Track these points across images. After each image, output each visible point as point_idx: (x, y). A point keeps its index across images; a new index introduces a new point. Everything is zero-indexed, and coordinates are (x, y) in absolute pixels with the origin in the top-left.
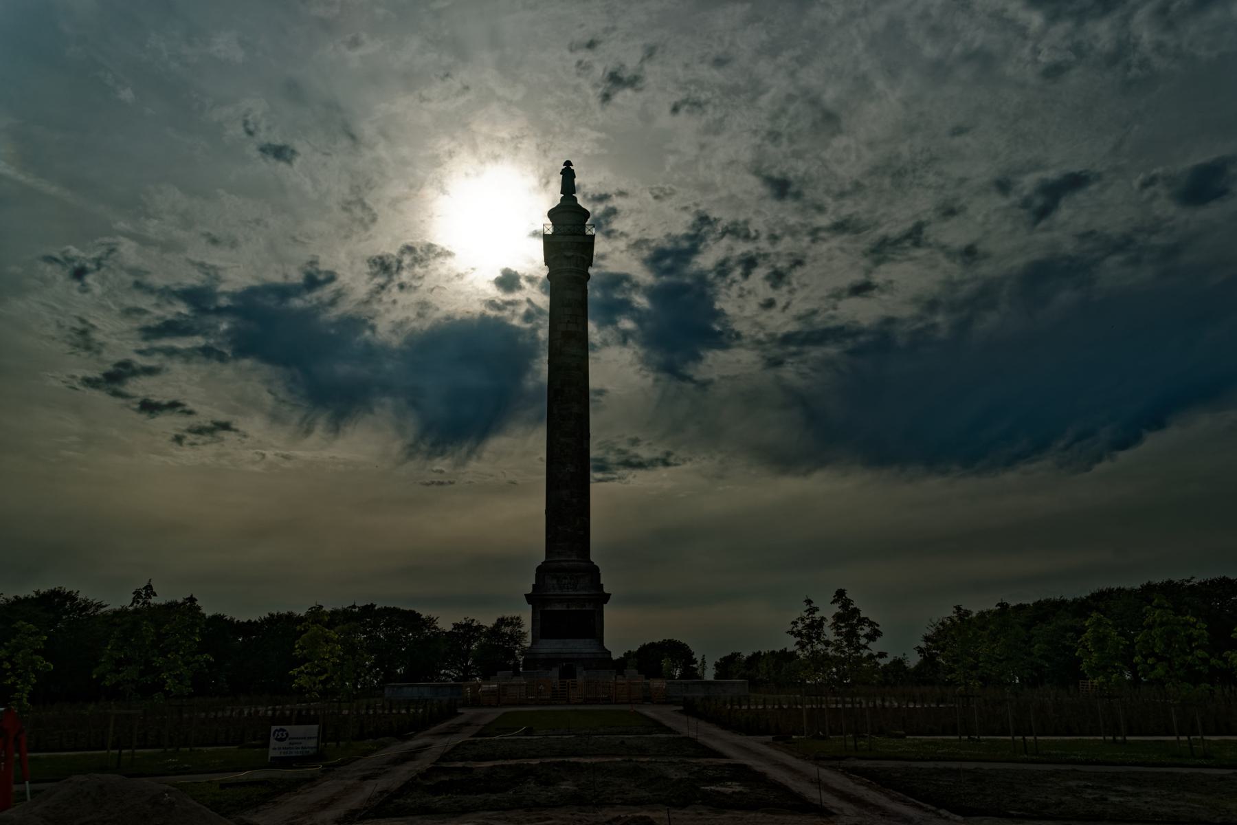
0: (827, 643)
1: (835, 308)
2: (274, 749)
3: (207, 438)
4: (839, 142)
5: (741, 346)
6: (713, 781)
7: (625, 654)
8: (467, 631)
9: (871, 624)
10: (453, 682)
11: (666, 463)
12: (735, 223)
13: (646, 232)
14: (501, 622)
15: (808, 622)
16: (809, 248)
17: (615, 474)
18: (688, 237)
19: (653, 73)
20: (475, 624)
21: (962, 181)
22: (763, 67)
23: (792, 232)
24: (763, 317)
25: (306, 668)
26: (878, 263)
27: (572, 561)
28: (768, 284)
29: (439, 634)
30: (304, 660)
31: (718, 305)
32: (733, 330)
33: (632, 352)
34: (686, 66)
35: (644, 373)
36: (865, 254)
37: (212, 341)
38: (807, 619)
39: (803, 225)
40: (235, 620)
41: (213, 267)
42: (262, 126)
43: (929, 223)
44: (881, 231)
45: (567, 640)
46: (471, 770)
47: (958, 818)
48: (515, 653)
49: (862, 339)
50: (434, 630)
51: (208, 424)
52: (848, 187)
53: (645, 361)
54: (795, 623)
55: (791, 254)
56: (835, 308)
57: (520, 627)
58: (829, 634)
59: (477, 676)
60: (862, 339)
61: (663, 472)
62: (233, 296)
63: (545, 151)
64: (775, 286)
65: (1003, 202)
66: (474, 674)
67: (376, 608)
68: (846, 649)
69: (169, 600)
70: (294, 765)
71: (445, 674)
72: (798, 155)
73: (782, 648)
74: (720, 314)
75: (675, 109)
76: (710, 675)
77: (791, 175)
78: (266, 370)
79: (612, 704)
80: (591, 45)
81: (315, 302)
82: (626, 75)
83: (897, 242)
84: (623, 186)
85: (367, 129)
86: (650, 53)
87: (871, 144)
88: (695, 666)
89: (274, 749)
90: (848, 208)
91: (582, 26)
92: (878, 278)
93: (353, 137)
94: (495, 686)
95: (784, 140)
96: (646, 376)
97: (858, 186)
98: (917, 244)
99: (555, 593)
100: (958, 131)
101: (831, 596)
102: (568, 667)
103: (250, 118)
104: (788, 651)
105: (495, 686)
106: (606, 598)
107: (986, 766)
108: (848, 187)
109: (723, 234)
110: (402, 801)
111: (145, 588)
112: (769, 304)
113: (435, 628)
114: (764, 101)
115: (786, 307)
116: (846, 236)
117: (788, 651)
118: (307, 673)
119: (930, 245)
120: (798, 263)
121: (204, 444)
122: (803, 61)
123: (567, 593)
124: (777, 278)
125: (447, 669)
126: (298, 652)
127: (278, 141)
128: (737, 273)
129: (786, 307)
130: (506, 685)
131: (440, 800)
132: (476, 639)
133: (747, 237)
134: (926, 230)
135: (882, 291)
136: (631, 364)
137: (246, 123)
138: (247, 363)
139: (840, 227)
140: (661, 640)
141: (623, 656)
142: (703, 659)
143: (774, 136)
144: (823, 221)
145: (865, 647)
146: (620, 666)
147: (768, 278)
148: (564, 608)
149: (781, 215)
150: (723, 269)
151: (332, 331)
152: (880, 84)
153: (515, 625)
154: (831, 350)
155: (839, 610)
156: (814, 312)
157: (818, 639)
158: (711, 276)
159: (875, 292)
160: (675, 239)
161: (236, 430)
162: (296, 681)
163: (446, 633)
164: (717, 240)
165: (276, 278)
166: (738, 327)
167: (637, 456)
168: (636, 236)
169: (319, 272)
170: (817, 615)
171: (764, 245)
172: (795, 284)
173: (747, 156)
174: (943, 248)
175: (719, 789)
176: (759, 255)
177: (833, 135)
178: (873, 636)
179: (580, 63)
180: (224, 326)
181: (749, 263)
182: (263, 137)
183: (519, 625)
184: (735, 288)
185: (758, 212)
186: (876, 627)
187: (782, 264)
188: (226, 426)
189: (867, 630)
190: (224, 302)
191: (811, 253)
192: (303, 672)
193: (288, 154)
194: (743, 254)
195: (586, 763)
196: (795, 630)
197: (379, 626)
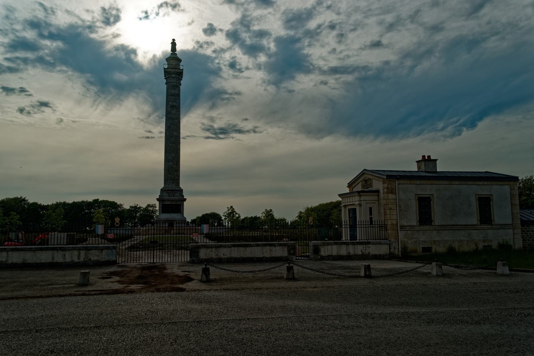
7: (197, 217)
8: (135, 209)
9: (238, 214)
11: (255, 132)
15: (227, 213)
20: (138, 206)
27: (173, 187)
29: (124, 210)
40: (42, 205)
45: (171, 214)
48: (154, 217)
50: (122, 209)
54: (224, 213)
60: (370, 73)
64: (340, 42)
67: (99, 200)
69: (15, 197)
73: (255, 215)
92: (385, 41)
102: (171, 223)
104: (257, 217)
113: (123, 208)
117: (257, 217)
140: (210, 213)
141: (196, 218)
148: (170, 203)
154: (349, 78)
163: (127, 210)
183: (155, 207)
197: (101, 207)
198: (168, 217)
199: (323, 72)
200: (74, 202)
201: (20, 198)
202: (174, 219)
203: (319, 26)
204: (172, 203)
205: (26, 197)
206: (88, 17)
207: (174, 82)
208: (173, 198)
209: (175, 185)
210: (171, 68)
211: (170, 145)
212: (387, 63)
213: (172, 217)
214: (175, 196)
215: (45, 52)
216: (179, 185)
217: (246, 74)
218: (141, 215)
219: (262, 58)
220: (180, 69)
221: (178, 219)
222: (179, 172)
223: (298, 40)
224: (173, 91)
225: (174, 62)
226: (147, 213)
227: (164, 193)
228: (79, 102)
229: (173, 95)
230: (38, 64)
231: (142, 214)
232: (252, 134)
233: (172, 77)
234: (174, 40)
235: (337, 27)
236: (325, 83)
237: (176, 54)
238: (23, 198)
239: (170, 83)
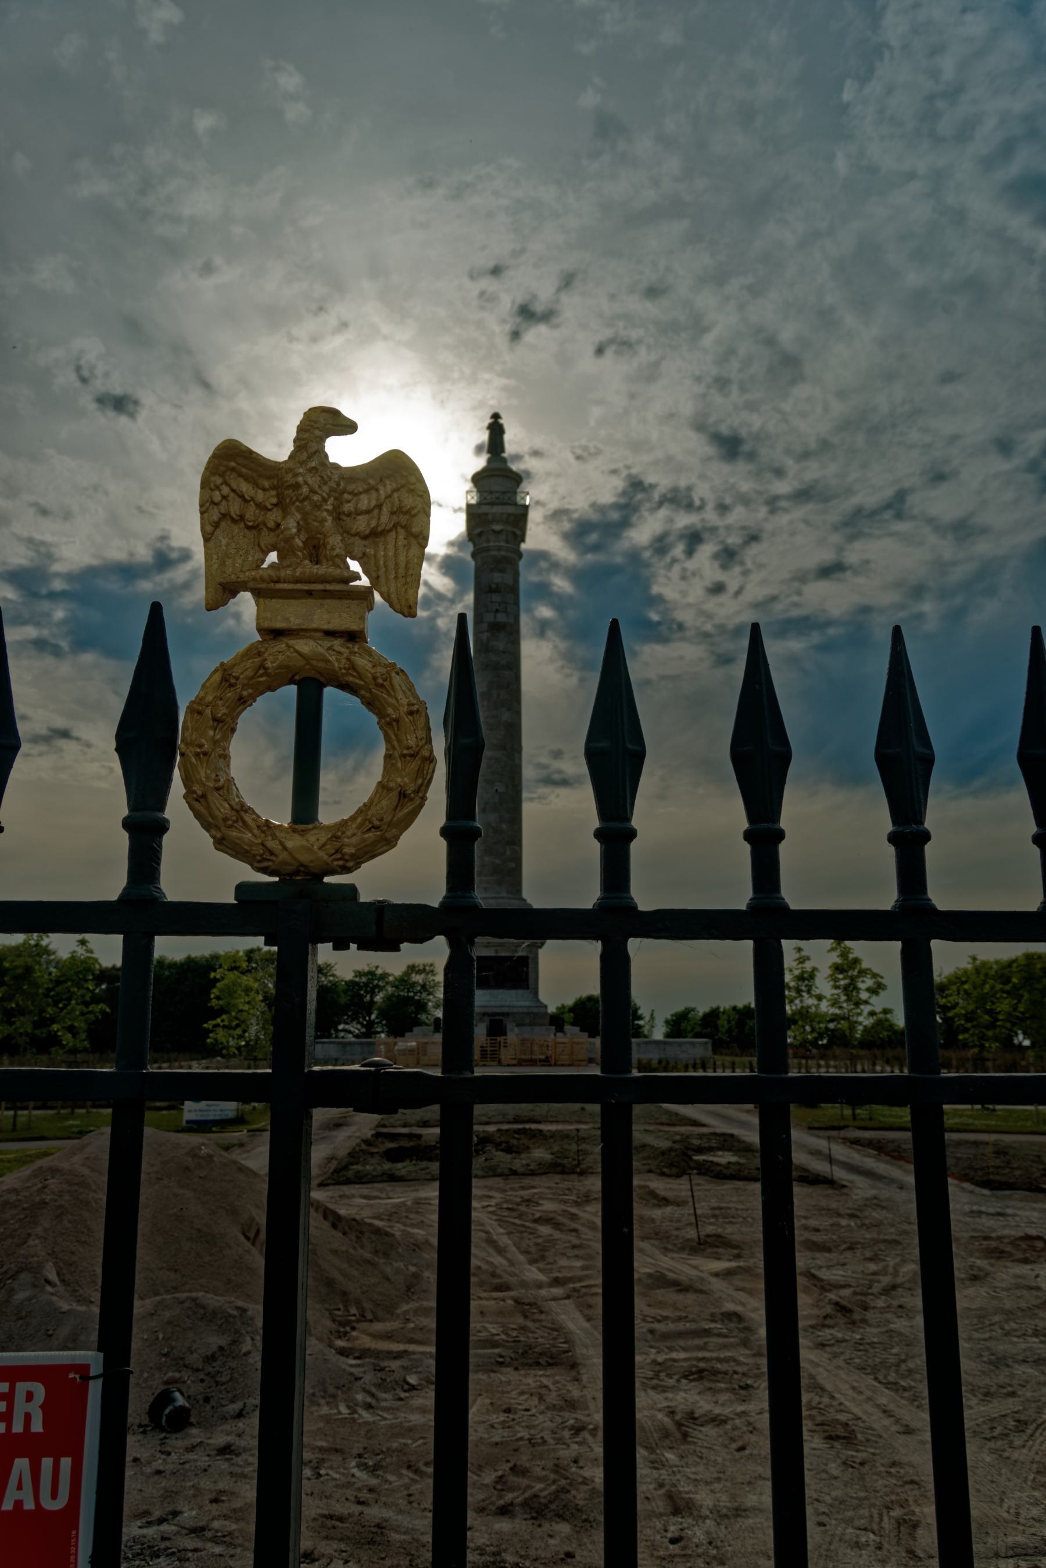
0: (820, 998)
1: (799, 593)
2: (190, 1111)
3: (43, 747)
4: (801, 391)
5: (684, 639)
6: (700, 1150)
9: (875, 975)
10: (353, 1039)
12: (675, 490)
13: (566, 500)
14: (412, 969)
15: (797, 972)
16: (766, 520)
17: (534, 792)
18: (616, 506)
19: (571, 305)
20: (379, 971)
21: (954, 439)
22: (707, 300)
23: (745, 500)
24: (711, 604)
25: (223, 1021)
26: (852, 538)
27: (503, 898)
28: (716, 564)
30: (222, 1011)
31: (655, 590)
32: (673, 621)
33: (551, 645)
34: (612, 297)
35: (567, 671)
36: (836, 528)
37: (45, 632)
39: (759, 493)
41: (43, 543)
42: (100, 369)
43: (912, 490)
44: (854, 501)
46: (419, 1136)
47: (986, 1192)
49: (832, 631)
50: (331, 978)
51: (44, 732)
52: (813, 445)
53: (568, 657)
55: (744, 528)
56: (799, 593)
57: (434, 975)
58: (823, 985)
59: (382, 1032)
62: (69, 577)
63: (442, 402)
64: (724, 567)
65: (1000, 465)
66: (379, 1029)
68: (845, 1005)
70: (214, 1129)
71: (344, 1030)
72: (752, 407)
74: (659, 599)
75: (600, 351)
76: (659, 1033)
77: (743, 432)
79: (550, 1065)
80: (496, 271)
81: (166, 585)
82: (539, 308)
83: (873, 513)
84: (538, 443)
85: (222, 376)
86: (567, 281)
87: (842, 394)
88: (641, 1023)
89: (190, 1111)
90: (813, 472)
91: (484, 248)
92: (852, 557)
93: (206, 385)
94: (414, 1044)
95: (735, 390)
96: (568, 676)
97: (825, 446)
98: (899, 516)
100: (949, 378)
103: (83, 362)
105: (414, 1044)
107: (1008, 1138)
108: (813, 445)
109: (660, 504)
110: (359, 1167)
112: (718, 589)
113: (333, 975)
114: (708, 340)
115: (738, 593)
116: (810, 506)
118: (224, 1027)
119: (914, 518)
120: (754, 538)
121: (41, 755)
122: (755, 291)
124: (728, 556)
125: (347, 1023)
126: (214, 1003)
127: (118, 391)
128: (678, 550)
129: (738, 593)
130: (427, 1043)
131: (404, 1167)
132: (381, 989)
133: (690, 507)
134: (912, 500)
135: (856, 572)
136: (551, 660)
137: (78, 369)
138: (88, 658)
139: (803, 495)
142: (652, 1015)
143: (722, 383)
144: (782, 487)
145: (866, 1002)
146: (557, 1021)
147: (716, 556)
149: (732, 480)
150: (661, 545)
151: (190, 620)
152: (850, 320)
153: (428, 973)
155: (839, 961)
156: (774, 599)
157: (809, 992)
158: (647, 554)
159: (848, 574)
160: (600, 509)
161: (78, 739)
162: (211, 1035)
164: (653, 510)
165: (117, 553)
166: (680, 616)
167: (560, 772)
168: (554, 505)
169: (171, 549)
170: (808, 966)
171: (711, 516)
172: (749, 564)
173: (688, 408)
174: (930, 521)
175: (711, 1159)
176: (705, 529)
177: (793, 382)
178: (874, 991)
179: (482, 294)
180: (59, 614)
181: (694, 539)
182: (99, 385)
183: (432, 972)
184: (677, 569)
185: (702, 477)
186: (880, 980)
187: (734, 540)
188: (65, 734)
189: (869, 982)
190: (58, 585)
191: (768, 527)
193: (130, 407)
194: (686, 527)
195: (549, 1131)
200: (189, 958)
202: (505, 1010)
207: (499, 549)
210: (492, 504)
218: (389, 998)
220: (515, 504)
221: (520, 1010)
222: (520, 846)
226: (409, 991)
229: (496, 590)
231: (393, 995)
234: (496, 416)
237: (504, 460)
239: (487, 549)
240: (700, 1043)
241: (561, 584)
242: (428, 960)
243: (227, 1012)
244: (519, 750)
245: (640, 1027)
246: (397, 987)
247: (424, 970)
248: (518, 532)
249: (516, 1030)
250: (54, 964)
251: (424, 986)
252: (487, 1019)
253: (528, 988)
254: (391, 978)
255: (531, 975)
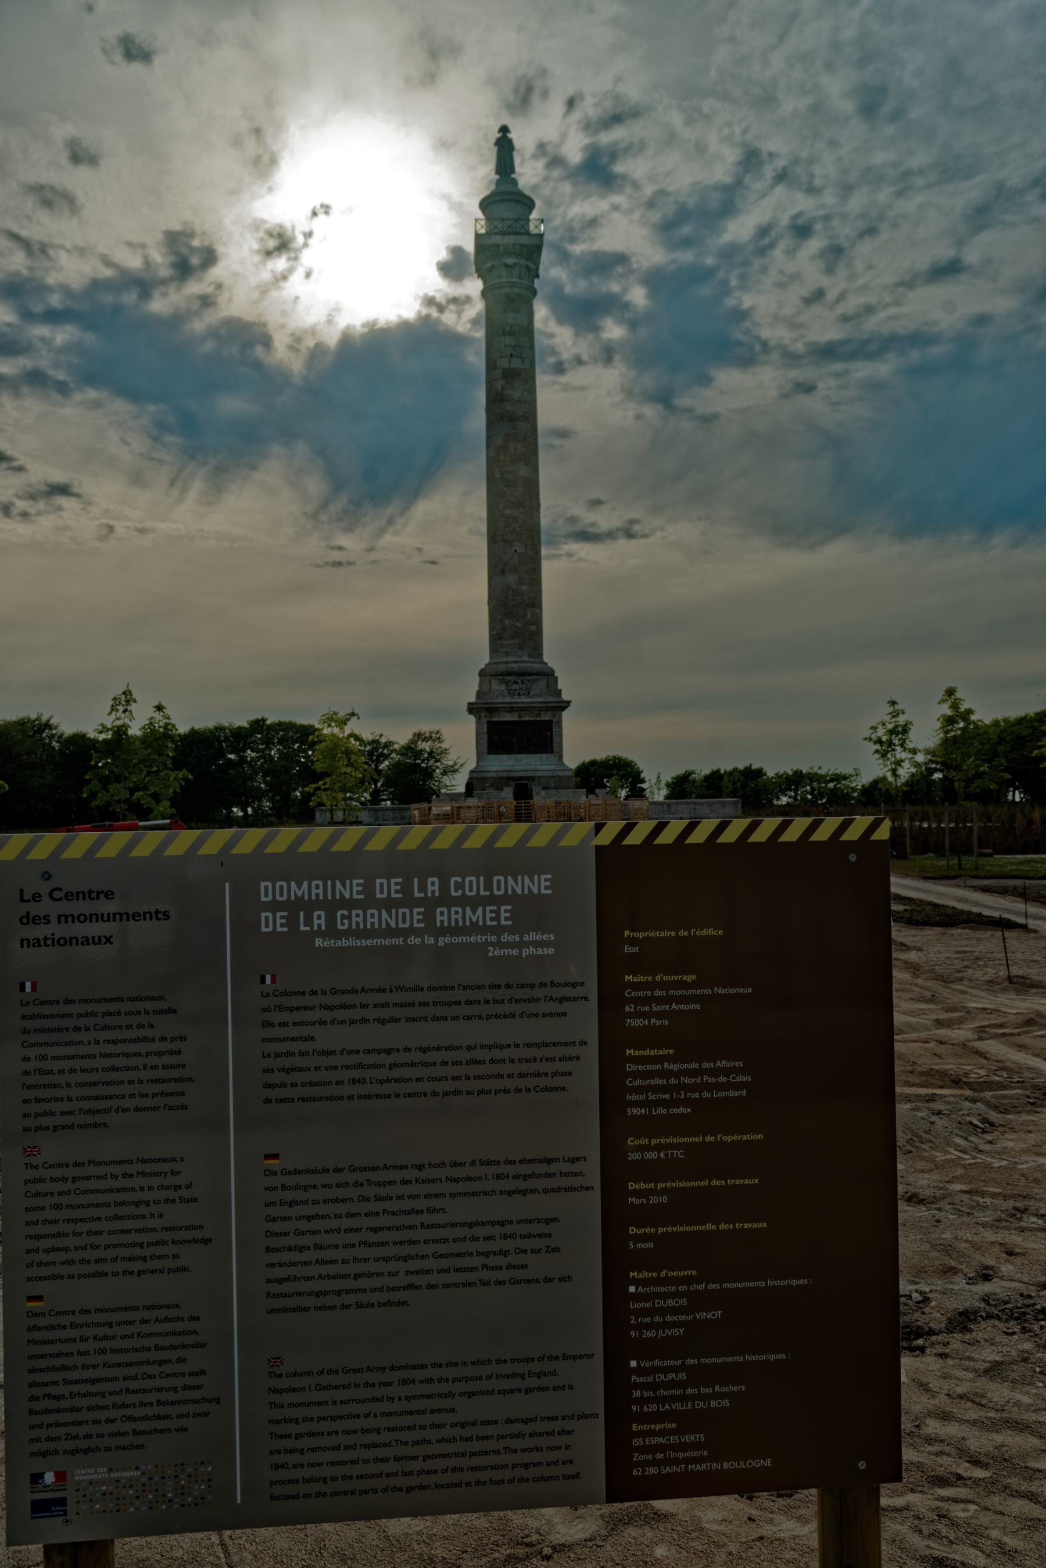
11: (630, 535)
15: (890, 727)
20: (383, 740)
23: (874, 177)
32: (758, 338)
38: (890, 723)
49: (936, 351)
54: (874, 728)
57: (441, 742)
59: (388, 800)
60: (936, 351)
61: (623, 543)
64: (829, 271)
73: (747, 764)
78: (120, 406)
88: (644, 786)
92: (971, 256)
99: (504, 700)
101: (940, 694)
106: (565, 705)
111: (124, 693)
123: (518, 700)
130: (459, 807)
132: (387, 757)
144: (920, 159)
147: (822, 255)
148: (516, 718)
154: (883, 369)
155: (949, 712)
161: (77, 496)
162: (313, 798)
170: (902, 719)
172: (859, 266)
181: (802, 230)
188: (63, 490)
190: (55, 300)
192: (319, 788)
196: (873, 736)
197: (273, 744)
198: (512, 768)
199: (791, 358)
200: (193, 729)
201: (36, 720)
202: (530, 774)
203: (763, 231)
204: (520, 717)
205: (52, 717)
206: (133, 262)
208: (524, 699)
209: (530, 656)
210: (503, 234)
211: (508, 512)
212: (982, 320)
213: (523, 768)
214: (531, 693)
215: (43, 362)
216: (541, 655)
217: (574, 377)
219: (613, 331)
220: (528, 233)
221: (545, 774)
222: (541, 609)
223: (704, 274)
224: (511, 318)
225: (508, 211)
227: (493, 681)
228: (137, 479)
230: (25, 389)
231: (399, 763)
232: (623, 543)
233: (506, 266)
235: (818, 227)
236: (808, 388)
238: (44, 718)
240: (730, 803)
241: (638, 296)
242: (434, 728)
243: (329, 775)
244: (538, 507)
245: (644, 790)
246: (402, 754)
247: (431, 737)
248: (532, 266)
249: (543, 793)
250: (56, 738)
251: (431, 753)
252: (512, 783)
253: (552, 752)
254: (396, 747)
255: (555, 739)
